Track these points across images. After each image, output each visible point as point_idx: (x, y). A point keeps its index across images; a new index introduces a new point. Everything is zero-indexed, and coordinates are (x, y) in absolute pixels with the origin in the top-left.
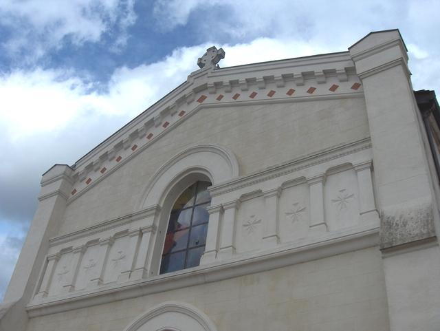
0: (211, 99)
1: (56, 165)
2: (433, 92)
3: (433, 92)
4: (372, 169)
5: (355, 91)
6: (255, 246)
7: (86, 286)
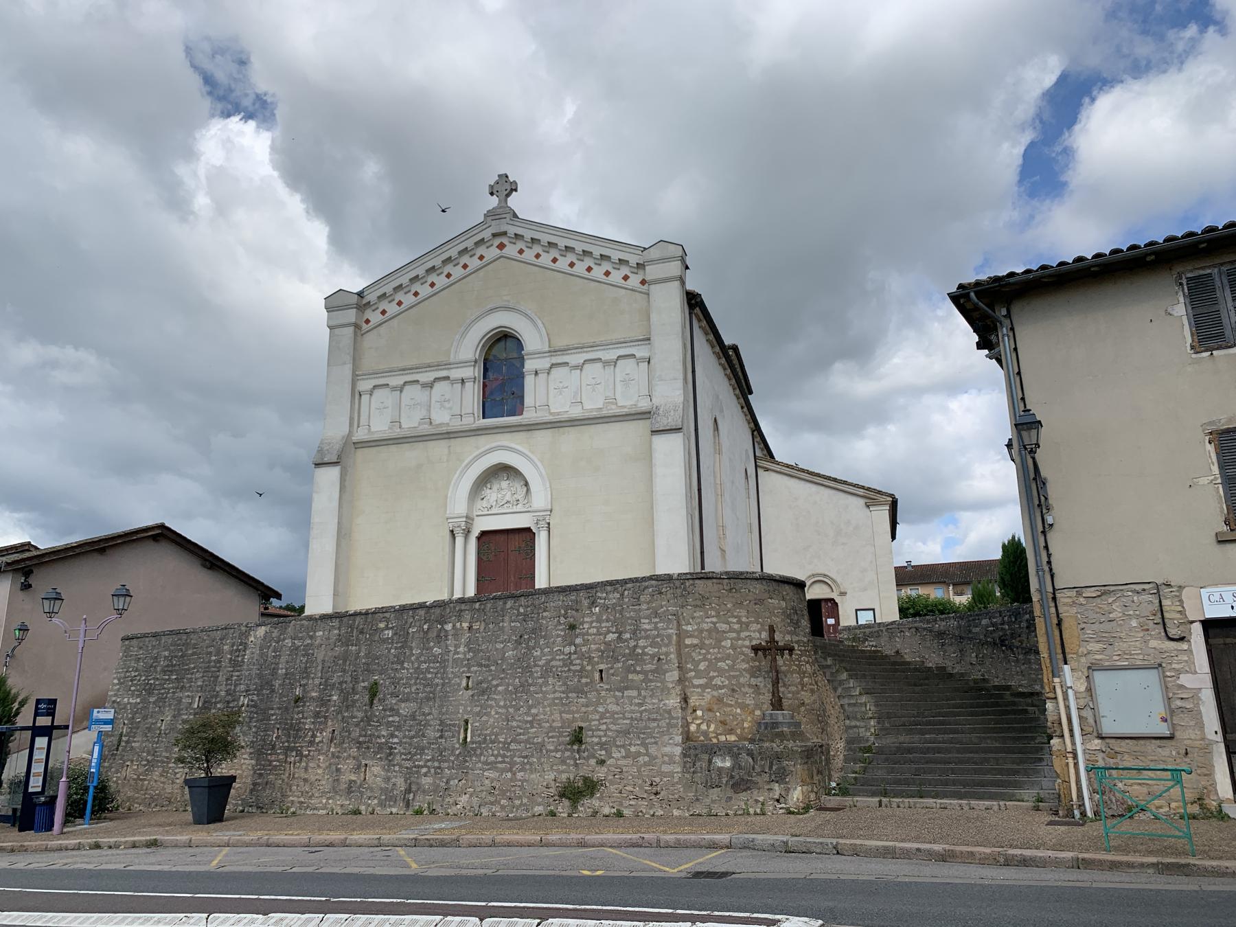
0: (511, 250)
1: (162, 535)
2: (978, 349)
3: (978, 349)
4: (649, 362)
5: (642, 287)
6: (562, 406)
7: (411, 422)
